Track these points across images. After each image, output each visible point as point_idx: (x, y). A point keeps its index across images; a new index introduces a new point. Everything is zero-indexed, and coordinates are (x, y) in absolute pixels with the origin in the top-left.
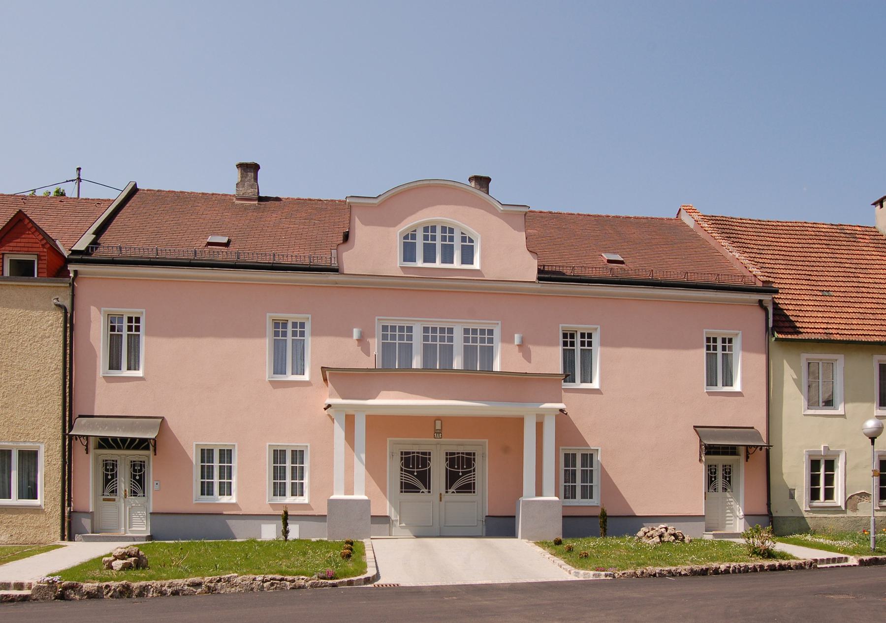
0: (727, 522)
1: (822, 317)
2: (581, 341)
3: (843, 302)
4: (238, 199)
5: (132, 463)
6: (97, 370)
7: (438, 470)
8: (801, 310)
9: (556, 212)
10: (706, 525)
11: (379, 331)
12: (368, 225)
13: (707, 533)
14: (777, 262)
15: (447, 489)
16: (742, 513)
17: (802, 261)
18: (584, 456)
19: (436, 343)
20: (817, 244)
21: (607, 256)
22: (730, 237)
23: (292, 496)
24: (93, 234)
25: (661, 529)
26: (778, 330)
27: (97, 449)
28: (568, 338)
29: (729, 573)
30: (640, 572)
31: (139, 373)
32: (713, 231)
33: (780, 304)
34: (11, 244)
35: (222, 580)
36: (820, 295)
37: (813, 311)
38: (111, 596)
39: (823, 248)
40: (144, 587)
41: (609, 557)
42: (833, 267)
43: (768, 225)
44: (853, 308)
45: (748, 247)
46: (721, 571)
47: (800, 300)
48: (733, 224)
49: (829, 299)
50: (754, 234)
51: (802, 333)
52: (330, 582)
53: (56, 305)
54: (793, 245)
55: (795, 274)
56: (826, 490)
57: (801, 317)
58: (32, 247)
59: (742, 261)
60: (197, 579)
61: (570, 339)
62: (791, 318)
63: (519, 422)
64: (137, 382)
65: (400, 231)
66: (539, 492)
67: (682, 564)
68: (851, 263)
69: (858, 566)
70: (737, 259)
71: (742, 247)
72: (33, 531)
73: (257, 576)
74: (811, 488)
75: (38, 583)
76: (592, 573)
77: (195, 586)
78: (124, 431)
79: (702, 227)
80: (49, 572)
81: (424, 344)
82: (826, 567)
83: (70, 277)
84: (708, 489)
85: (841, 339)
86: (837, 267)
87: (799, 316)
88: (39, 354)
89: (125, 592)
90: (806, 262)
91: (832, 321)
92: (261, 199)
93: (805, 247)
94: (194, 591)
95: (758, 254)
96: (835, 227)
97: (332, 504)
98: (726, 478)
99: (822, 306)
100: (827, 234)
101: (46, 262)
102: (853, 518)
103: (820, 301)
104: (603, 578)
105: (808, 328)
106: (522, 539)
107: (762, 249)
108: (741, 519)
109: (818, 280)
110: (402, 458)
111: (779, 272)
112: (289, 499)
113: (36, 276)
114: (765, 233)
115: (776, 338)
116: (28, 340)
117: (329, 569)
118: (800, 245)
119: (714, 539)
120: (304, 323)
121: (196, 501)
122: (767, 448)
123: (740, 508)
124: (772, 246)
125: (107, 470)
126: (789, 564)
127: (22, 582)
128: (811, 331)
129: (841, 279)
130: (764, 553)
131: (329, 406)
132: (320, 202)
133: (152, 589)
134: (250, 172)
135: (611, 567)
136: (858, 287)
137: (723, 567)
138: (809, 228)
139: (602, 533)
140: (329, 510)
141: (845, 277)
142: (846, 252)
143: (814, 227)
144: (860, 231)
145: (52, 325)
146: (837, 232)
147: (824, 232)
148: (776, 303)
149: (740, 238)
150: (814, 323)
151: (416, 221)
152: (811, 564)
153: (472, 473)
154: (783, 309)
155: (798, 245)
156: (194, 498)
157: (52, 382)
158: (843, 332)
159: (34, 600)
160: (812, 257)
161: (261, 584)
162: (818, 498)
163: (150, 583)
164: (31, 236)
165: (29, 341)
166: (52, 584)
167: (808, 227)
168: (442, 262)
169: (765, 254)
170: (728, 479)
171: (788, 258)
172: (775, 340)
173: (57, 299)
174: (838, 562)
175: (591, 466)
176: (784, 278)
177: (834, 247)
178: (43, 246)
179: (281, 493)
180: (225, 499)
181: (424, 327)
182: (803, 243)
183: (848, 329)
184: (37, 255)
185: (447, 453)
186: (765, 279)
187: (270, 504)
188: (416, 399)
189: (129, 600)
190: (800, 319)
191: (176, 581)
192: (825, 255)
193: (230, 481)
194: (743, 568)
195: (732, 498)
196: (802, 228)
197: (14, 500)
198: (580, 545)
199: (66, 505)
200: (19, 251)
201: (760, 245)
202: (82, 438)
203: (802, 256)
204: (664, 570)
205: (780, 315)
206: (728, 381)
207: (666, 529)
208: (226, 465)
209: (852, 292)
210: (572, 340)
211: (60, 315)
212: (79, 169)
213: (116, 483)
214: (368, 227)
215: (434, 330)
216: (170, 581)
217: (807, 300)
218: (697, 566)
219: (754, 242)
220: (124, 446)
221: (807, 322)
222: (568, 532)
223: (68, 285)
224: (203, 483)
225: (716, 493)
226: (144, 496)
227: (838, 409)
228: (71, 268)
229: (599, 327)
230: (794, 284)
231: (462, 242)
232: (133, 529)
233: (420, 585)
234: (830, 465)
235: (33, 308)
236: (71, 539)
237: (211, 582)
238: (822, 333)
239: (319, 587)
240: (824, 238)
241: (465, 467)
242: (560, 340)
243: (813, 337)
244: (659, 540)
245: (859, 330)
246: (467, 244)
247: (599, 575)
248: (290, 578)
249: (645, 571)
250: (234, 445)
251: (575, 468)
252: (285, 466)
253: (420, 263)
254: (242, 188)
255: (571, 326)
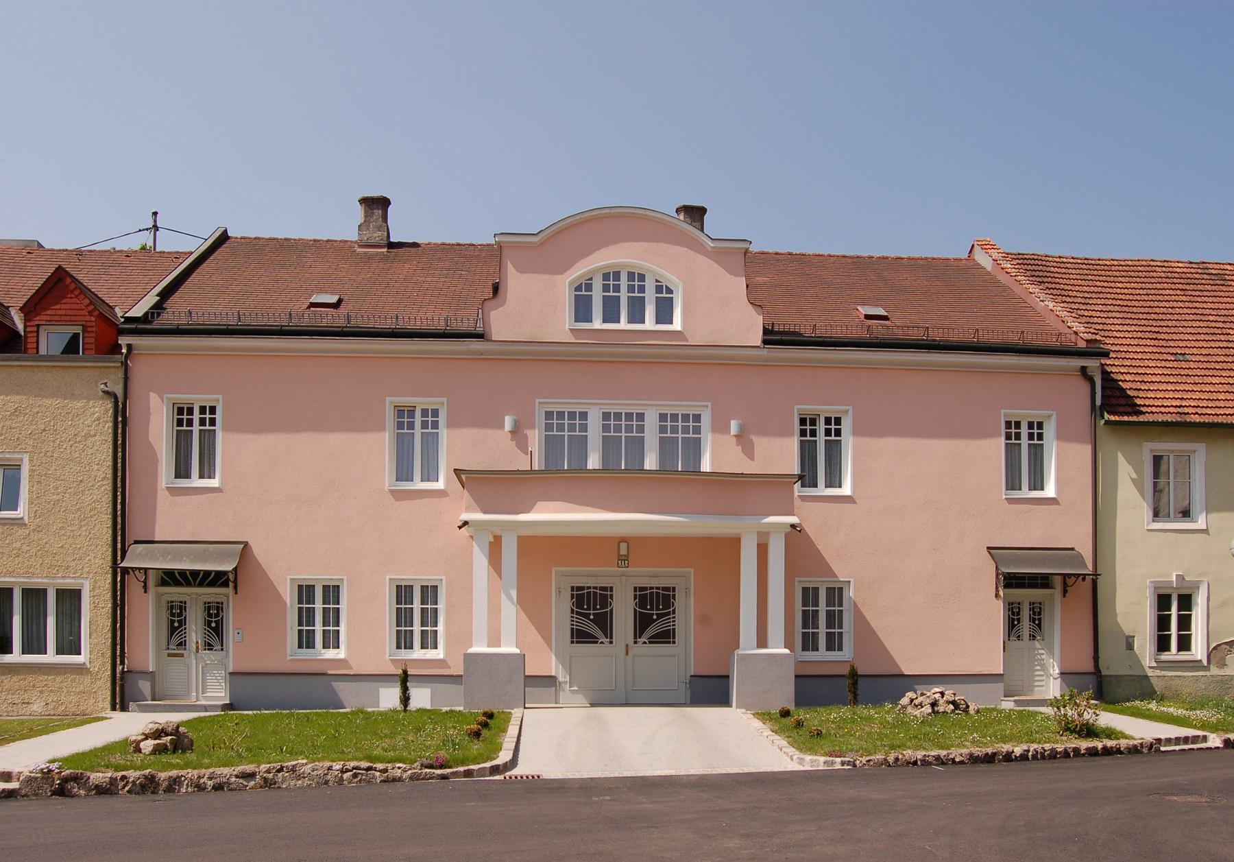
0: (1037, 684)
1: (1173, 391)
2: (200, 418)
3: (1205, 369)
4: (361, 246)
5: (169, 605)
6: (159, 479)
7: (623, 612)
8: (1143, 381)
9: (798, 253)
10: (1004, 687)
11: (540, 420)
12: (526, 272)
13: (1006, 699)
14: (1110, 315)
15: (635, 638)
16: (1057, 671)
17: (1147, 314)
18: (830, 591)
19: (677, 435)
20: (1169, 289)
21: (863, 310)
22: (1043, 282)
23: (422, 648)
24: (157, 295)
25: (934, 694)
26: (1109, 410)
27: (158, 586)
28: (807, 423)
29: (1028, 759)
30: (892, 758)
31: (214, 483)
32: (1018, 274)
33: (1113, 373)
34: (48, 312)
35: (285, 769)
36: (1171, 360)
37: (1160, 382)
38: (129, 792)
39: (1177, 295)
40: (175, 779)
41: (852, 735)
42: (1191, 321)
43: (1099, 265)
44: (1219, 377)
45: (1068, 296)
46: (1015, 756)
47: (1142, 367)
48: (1048, 264)
49: (1184, 365)
50: (1078, 277)
51: (1144, 413)
52: (439, 772)
53: (104, 392)
54: (1134, 292)
55: (1135, 331)
56: (1180, 637)
57: (1143, 390)
58: (75, 315)
59: (1058, 313)
60: (249, 768)
61: (1015, 429)
62: (1129, 392)
63: (734, 543)
64: (212, 494)
65: (569, 280)
66: (762, 642)
67: (958, 746)
68: (1218, 315)
69: (1223, 748)
70: (1051, 310)
71: (1058, 293)
72: (75, 699)
73: (334, 764)
74: (1158, 635)
75: (30, 772)
76: (822, 759)
77: (247, 777)
78: (193, 561)
79: (1003, 268)
80: (51, 757)
81: (603, 436)
82: (1174, 751)
83: (122, 353)
84: (1009, 636)
85: (1202, 421)
86: (1197, 320)
87: (1141, 389)
88: (81, 458)
89: (149, 785)
90: (1152, 315)
91: (1189, 395)
92: (391, 245)
93: (1150, 294)
94: (244, 785)
95: (1083, 304)
96: (1194, 266)
97: (470, 659)
98: (1034, 621)
99: (1173, 375)
100: (1183, 276)
101: (94, 335)
102: (1221, 678)
103: (1171, 368)
104: (838, 766)
105: (1154, 406)
106: (737, 708)
107: (1089, 298)
108: (1058, 678)
109: (1168, 340)
110: (572, 595)
111: (1113, 329)
112: (417, 653)
113: (81, 354)
114: (1094, 275)
115: (1105, 421)
116: (68, 440)
117: (442, 753)
118: (1145, 292)
119: (1015, 708)
120: (438, 409)
121: (291, 656)
122: (1094, 577)
123: (1055, 663)
124: (1103, 293)
125: (173, 615)
126: (1118, 746)
127: (11, 771)
128: (1158, 410)
129: (1202, 337)
130: (1081, 730)
131: (466, 523)
132: (472, 248)
133: (186, 781)
134: (379, 209)
135: (852, 750)
136: (1227, 347)
137: (1018, 751)
138: (1157, 268)
139: (850, 700)
140: (466, 669)
141: (1208, 334)
142: (1211, 299)
143: (1164, 266)
144: (1231, 270)
145: (98, 419)
146: (1198, 273)
147: (1178, 273)
148: (1107, 372)
149: (1058, 283)
150: (1163, 399)
151: (591, 265)
152: (1151, 745)
153: (671, 616)
154: (1117, 381)
155: (1141, 292)
156: (289, 652)
157: (99, 497)
158: (1204, 411)
159: (23, 796)
160: (1162, 307)
161: (340, 775)
162: (1168, 649)
163: (183, 772)
164: (74, 300)
165: (69, 441)
166: (47, 774)
167: (1155, 266)
168: (629, 322)
169: (1092, 304)
170: (1037, 622)
171: (1126, 309)
172: (1105, 424)
173: (105, 384)
174: (1192, 743)
175: (841, 605)
176: (1120, 337)
177: (1194, 293)
178: (90, 313)
179: (408, 645)
180: (331, 654)
181: (603, 413)
182: (1149, 289)
183: (1212, 407)
184: (83, 325)
185: (635, 589)
186: (1090, 337)
187: (392, 660)
188: (574, 511)
189: (155, 797)
190: (1141, 394)
191: (219, 771)
192: (1180, 304)
193: (337, 628)
194: (1048, 752)
195: (1043, 649)
196: (1147, 269)
197: (50, 657)
198: (813, 717)
199: (119, 663)
200: (58, 321)
201: (1086, 292)
202: (137, 572)
203: (1146, 307)
204: (929, 756)
205: (1113, 388)
206: (1037, 483)
207: (942, 694)
208: (331, 606)
209: (1218, 355)
210: (837, 427)
211: (110, 405)
212: (155, 214)
213: (185, 633)
214: (525, 276)
215: (618, 416)
216: (211, 770)
217: (1152, 367)
218: (980, 749)
219: (1077, 288)
220: (195, 581)
221: (1151, 398)
222: (802, 699)
223: (120, 364)
224: (300, 632)
225: (1020, 641)
226: (222, 650)
227: (1197, 522)
228: (123, 341)
229: (851, 408)
230: (1134, 345)
231: (656, 293)
232: (208, 694)
233: (571, 777)
234: (1186, 602)
235: (73, 397)
236: (124, 708)
237: (268, 771)
238: (1174, 413)
239: (422, 779)
240: (1179, 281)
241: (661, 607)
242: (796, 428)
243: (1160, 418)
244: (930, 711)
245: (1228, 408)
246: (664, 295)
247: (833, 763)
248: (380, 766)
249: (900, 757)
250: (343, 579)
251: (817, 608)
252: (437, 608)
253: (597, 324)
254: (366, 231)
255: (810, 408)
